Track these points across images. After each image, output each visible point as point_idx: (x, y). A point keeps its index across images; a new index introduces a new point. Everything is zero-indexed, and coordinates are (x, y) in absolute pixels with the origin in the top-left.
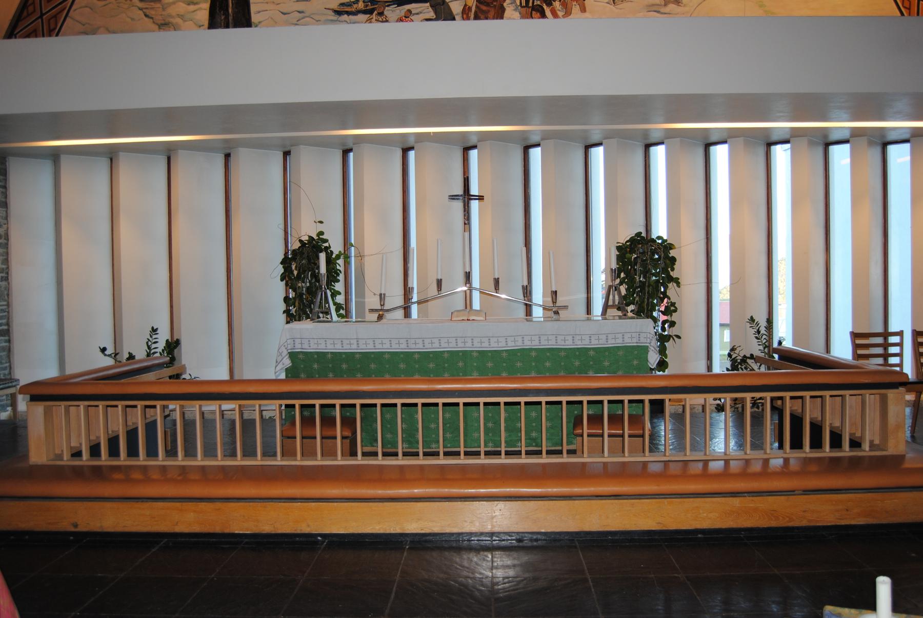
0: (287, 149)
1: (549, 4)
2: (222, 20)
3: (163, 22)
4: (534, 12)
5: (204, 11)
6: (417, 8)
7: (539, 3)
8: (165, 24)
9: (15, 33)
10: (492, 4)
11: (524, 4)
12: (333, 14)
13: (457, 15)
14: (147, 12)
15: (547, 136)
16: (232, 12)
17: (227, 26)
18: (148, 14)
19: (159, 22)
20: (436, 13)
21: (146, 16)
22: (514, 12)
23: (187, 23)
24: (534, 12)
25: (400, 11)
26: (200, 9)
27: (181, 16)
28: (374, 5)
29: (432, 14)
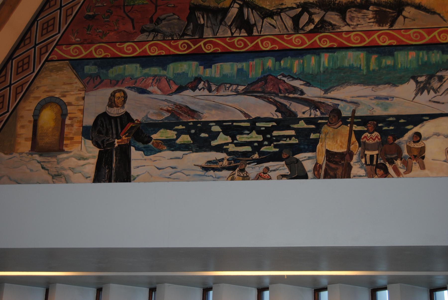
0: (153, 286)
1: (391, 162)
2: (106, 173)
3: (56, 173)
4: (378, 170)
5: (92, 165)
6: (274, 166)
7: (382, 161)
8: (58, 175)
9: (38, 20)
10: (340, 162)
11: (368, 162)
12: (201, 170)
13: (309, 171)
14: (45, 165)
15: (393, 280)
16: (115, 167)
17: (110, 181)
18: (44, 166)
19: (53, 174)
20: (290, 170)
21: (43, 168)
22: (360, 169)
23: (77, 174)
24: (378, 170)
25: (259, 168)
26: (89, 163)
27: (72, 169)
28: (236, 163)
29: (286, 171)
